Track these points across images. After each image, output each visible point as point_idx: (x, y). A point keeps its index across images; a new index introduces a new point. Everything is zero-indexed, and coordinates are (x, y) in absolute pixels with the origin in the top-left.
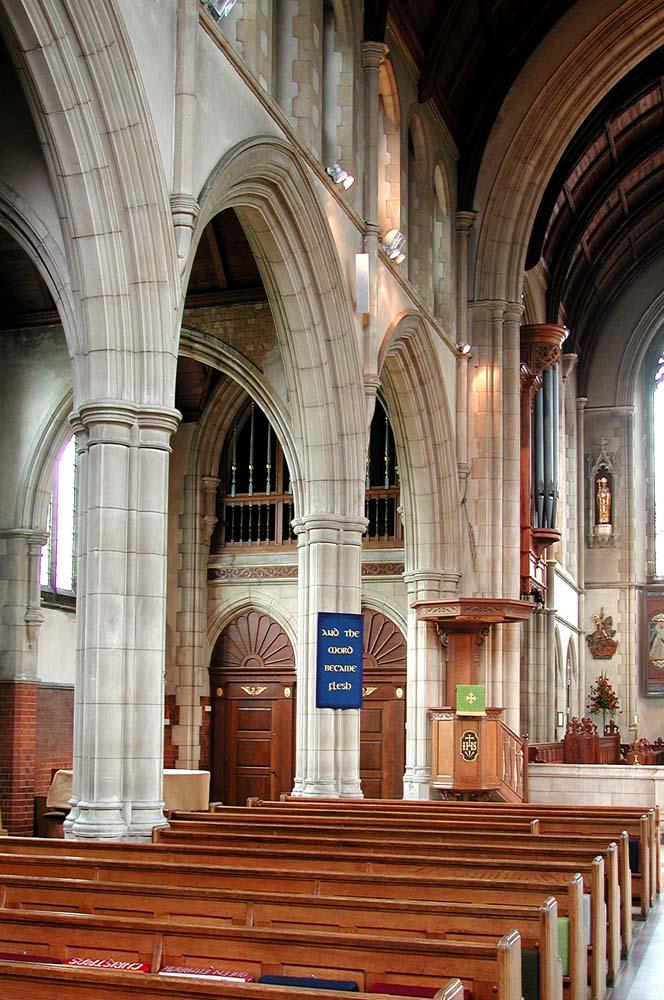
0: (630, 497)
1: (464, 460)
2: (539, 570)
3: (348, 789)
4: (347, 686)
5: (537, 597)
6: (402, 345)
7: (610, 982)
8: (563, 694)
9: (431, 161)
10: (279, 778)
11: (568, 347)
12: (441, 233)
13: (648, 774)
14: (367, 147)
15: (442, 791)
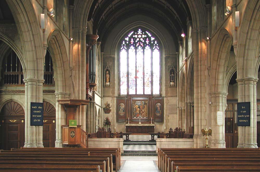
3: (40, 145)
4: (39, 120)
5: (90, 100)
6: (54, 37)
8: (97, 122)
12: (65, 10)
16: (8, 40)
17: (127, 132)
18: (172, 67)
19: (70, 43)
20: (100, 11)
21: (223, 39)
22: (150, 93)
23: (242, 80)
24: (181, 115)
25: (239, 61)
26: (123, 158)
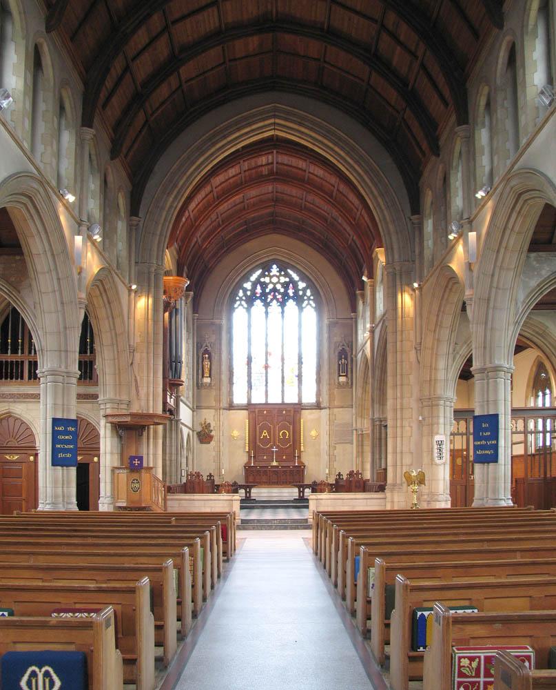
0: (220, 365)
1: (132, 343)
2: (172, 400)
3: (70, 506)
4: (69, 455)
5: (171, 413)
6: (98, 283)
7: (212, 587)
8: (184, 461)
9: (117, 191)
10: (27, 502)
11: (188, 289)
12: (121, 226)
13: (229, 498)
14: (82, 181)
15: (120, 507)
16: (8, 290)
17: (246, 482)
18: (343, 345)
19: (129, 295)
20: (193, 227)
21: (447, 287)
22: (296, 401)
23: (482, 370)
24: (361, 445)
25: (476, 330)
26: (240, 534)
